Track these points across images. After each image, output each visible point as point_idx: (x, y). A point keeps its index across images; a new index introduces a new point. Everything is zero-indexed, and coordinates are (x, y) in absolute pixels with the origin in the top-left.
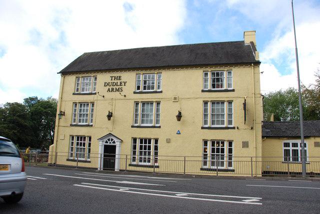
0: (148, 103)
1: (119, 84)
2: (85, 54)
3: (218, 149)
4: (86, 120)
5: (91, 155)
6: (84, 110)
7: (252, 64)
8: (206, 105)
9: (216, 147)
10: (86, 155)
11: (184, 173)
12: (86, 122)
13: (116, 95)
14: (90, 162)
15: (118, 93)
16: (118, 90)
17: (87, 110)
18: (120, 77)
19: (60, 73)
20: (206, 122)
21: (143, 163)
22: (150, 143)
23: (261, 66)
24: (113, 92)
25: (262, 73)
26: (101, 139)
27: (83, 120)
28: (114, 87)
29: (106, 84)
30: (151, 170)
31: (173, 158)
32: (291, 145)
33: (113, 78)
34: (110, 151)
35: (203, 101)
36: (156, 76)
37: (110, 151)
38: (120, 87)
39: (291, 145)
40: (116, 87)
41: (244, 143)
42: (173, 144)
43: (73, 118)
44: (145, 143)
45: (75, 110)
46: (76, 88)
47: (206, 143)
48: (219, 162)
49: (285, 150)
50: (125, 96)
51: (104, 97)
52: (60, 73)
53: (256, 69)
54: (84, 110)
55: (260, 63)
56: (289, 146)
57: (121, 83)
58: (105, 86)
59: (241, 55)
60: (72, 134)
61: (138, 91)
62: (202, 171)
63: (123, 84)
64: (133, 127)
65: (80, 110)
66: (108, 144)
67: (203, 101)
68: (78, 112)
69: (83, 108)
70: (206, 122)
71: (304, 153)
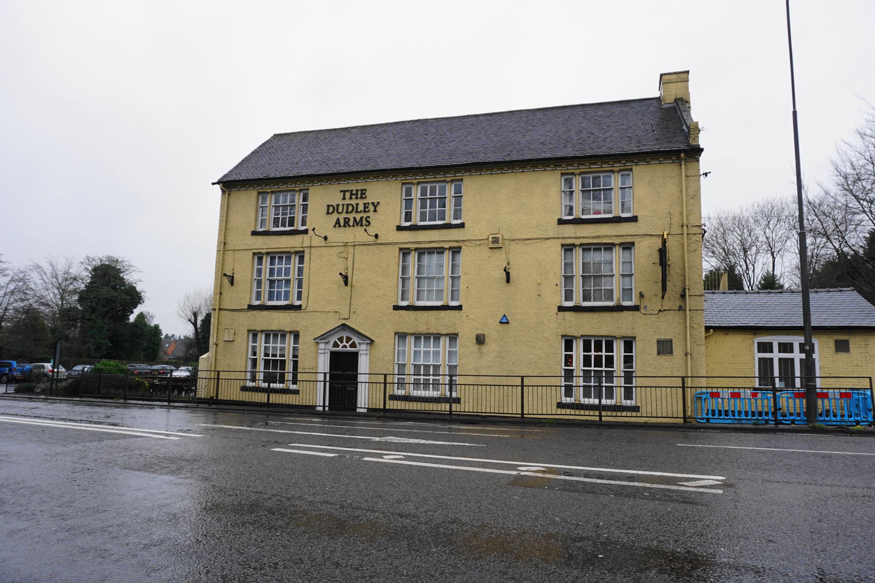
0: (431, 251)
1: (361, 208)
2: (276, 136)
3: (598, 360)
4: (287, 294)
5: (300, 377)
6: (280, 270)
7: (682, 155)
8: (569, 253)
9: (604, 353)
10: (289, 377)
11: (522, 414)
12: (286, 298)
13: (357, 234)
14: (296, 392)
15: (359, 230)
16: (358, 223)
17: (287, 271)
18: (363, 192)
19: (218, 183)
20: (569, 296)
21: (421, 393)
22: (610, 348)
23: (702, 158)
24: (348, 228)
25: (706, 174)
26: (324, 337)
27: (279, 293)
28: (351, 217)
29: (331, 209)
30: (445, 407)
31: (497, 381)
32: (776, 348)
33: (348, 195)
34: (344, 366)
35: (562, 246)
36: (450, 191)
37: (344, 366)
38: (365, 215)
39: (776, 348)
40: (354, 215)
41: (659, 342)
42: (491, 347)
43: (255, 289)
44: (598, 348)
45: (259, 272)
46: (260, 218)
47: (569, 346)
48: (600, 387)
49: (760, 359)
50: (376, 236)
51: (326, 238)
52: (218, 183)
53: (691, 165)
54: (280, 270)
55: (702, 150)
56: (792, 351)
57: (366, 206)
58: (328, 213)
59: (665, 133)
60: (253, 328)
61: (408, 224)
62: (559, 411)
63: (371, 208)
64: (396, 308)
65: (272, 271)
66: (340, 349)
67: (562, 246)
68: (265, 275)
69: (276, 266)
70: (569, 296)
71: (808, 365)
